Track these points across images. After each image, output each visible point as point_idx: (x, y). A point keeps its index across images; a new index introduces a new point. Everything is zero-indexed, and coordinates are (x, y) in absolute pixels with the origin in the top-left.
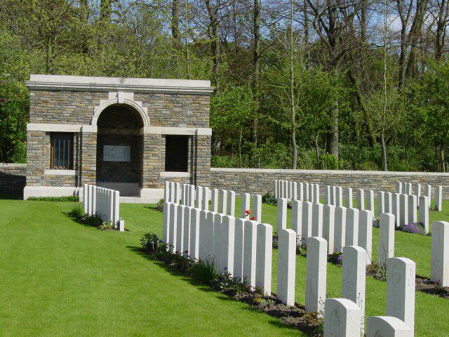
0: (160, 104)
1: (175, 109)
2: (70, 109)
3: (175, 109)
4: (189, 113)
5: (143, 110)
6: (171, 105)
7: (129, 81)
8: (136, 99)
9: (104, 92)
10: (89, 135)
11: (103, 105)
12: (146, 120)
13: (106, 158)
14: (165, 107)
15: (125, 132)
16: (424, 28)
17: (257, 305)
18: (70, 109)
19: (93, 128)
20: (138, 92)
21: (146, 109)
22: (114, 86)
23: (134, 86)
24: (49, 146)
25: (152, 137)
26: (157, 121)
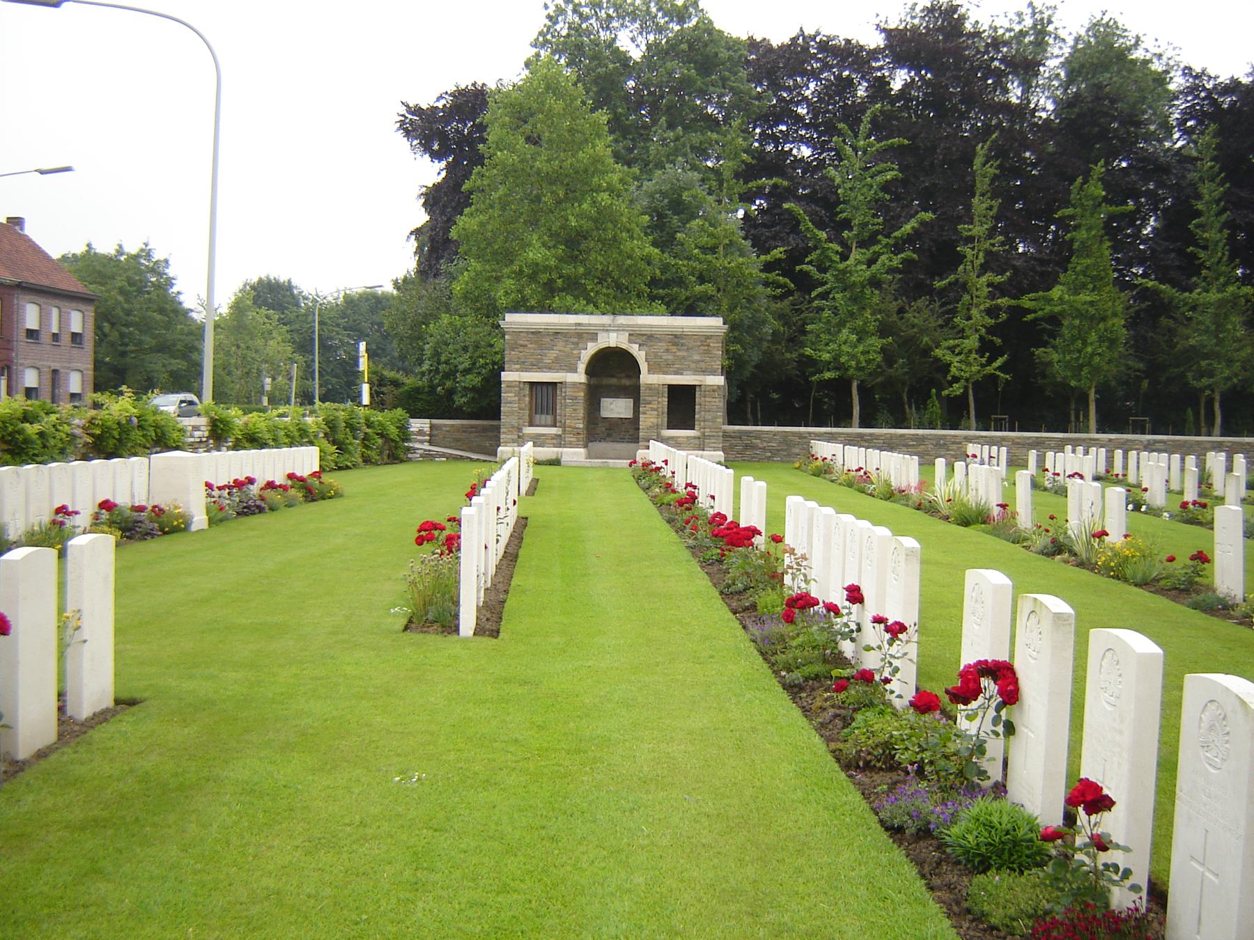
0: (661, 346)
1: (679, 354)
2: (552, 354)
3: (679, 354)
4: (696, 357)
5: (639, 354)
6: (674, 349)
7: (622, 320)
8: (630, 341)
9: (594, 337)
10: (574, 384)
11: (592, 349)
12: (644, 367)
13: (605, 413)
14: (667, 351)
15: (626, 382)
16: (1184, 142)
17: (676, 299)
18: (552, 354)
19: (580, 377)
20: (634, 336)
21: (643, 354)
22: (604, 325)
23: (628, 326)
24: (527, 399)
25: (650, 387)
26: (654, 368)
